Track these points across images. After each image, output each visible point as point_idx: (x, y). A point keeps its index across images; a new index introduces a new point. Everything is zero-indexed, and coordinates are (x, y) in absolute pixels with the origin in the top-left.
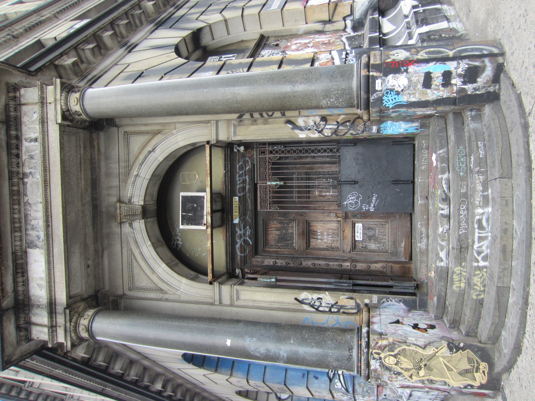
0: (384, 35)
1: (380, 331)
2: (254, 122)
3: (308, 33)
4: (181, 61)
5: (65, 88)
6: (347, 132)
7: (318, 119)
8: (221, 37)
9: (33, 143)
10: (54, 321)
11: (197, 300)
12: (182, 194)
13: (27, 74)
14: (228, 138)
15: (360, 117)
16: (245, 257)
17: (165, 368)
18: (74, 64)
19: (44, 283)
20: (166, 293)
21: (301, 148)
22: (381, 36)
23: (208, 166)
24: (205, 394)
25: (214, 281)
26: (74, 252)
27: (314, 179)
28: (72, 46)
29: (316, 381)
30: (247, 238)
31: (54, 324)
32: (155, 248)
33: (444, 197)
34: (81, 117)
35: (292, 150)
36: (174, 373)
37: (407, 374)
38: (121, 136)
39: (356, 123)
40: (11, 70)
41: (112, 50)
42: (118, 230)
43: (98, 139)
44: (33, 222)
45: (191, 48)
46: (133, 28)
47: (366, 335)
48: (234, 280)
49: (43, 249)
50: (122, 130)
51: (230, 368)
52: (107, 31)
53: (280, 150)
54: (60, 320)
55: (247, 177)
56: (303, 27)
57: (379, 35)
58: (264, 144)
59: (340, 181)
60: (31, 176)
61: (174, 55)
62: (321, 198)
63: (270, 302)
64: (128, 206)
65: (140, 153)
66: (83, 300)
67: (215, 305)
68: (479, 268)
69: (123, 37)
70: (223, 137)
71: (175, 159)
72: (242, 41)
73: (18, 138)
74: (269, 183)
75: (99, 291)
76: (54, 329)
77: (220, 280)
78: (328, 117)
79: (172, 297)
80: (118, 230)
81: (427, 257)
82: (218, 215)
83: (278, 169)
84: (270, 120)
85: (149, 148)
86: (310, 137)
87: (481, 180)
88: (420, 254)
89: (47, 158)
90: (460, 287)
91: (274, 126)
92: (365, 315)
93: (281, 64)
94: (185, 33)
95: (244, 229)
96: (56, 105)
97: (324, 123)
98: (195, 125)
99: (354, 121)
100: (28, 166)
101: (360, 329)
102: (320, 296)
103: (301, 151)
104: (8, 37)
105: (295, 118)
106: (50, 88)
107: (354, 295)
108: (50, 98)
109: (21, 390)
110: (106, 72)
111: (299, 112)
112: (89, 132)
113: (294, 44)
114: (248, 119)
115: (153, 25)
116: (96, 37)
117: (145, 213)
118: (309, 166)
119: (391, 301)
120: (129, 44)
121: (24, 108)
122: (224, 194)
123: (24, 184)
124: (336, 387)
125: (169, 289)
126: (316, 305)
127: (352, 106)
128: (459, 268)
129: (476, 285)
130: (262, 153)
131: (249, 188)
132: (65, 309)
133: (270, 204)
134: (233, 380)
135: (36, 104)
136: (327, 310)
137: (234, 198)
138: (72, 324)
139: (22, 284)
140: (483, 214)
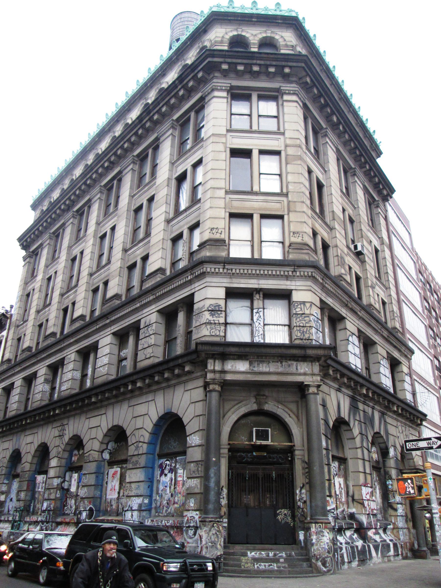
2: (303, 468)
3: (347, 486)
7: (305, 499)
8: (345, 435)
12: (270, 429)
19: (234, 369)
37: (209, 538)
42: (252, 395)
44: (261, 365)
46: (348, 387)
50: (299, 400)
55: (275, 460)
56: (351, 484)
72: (343, 447)
83: (280, 476)
91: (301, 478)
108: (315, 378)
113: (341, 480)
115: (352, 394)
121: (310, 363)
123: (277, 362)
135: (312, 371)
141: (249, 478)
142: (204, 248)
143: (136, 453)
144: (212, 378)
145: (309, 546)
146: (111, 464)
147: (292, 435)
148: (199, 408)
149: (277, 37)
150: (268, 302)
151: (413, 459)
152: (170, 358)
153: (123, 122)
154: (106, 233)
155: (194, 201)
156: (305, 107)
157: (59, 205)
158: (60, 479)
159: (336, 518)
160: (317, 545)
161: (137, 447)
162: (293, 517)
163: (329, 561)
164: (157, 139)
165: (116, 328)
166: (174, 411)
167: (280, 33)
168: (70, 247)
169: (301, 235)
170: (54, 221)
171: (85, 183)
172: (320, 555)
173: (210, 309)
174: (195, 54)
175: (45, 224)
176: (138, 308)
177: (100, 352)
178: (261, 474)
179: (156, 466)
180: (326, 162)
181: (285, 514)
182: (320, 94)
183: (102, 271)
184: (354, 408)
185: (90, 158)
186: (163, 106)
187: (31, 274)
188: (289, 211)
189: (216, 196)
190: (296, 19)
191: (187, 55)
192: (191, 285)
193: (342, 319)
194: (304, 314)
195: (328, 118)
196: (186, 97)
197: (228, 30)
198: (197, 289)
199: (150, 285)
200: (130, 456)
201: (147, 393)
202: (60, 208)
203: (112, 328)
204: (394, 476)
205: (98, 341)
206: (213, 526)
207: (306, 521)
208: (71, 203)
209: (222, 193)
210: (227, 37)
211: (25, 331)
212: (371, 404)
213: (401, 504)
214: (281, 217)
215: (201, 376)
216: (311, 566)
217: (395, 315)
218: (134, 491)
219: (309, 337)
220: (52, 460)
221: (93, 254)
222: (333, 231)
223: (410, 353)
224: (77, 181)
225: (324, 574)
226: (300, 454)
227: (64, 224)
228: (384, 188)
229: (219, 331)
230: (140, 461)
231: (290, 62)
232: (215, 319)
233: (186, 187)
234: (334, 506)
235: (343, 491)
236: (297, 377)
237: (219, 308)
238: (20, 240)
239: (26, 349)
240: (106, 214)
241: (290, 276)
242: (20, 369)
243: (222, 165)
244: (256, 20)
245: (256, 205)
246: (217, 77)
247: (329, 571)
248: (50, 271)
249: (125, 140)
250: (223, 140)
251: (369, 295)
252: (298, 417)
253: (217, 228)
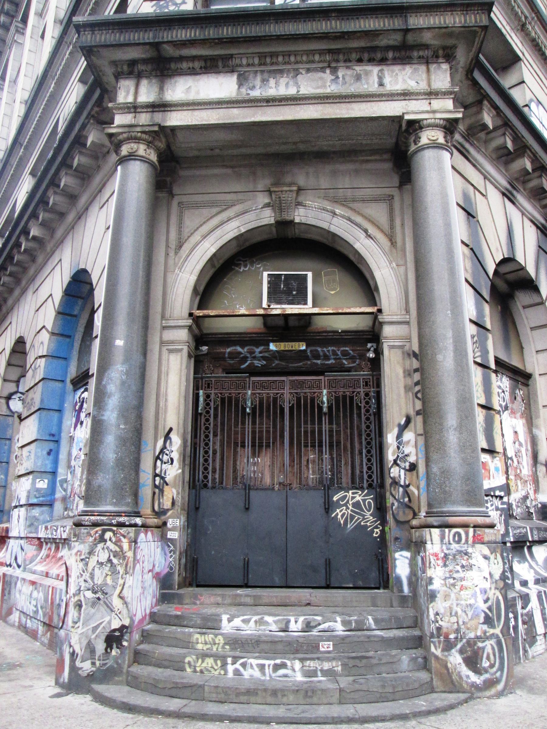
0: (530, 548)
1: (139, 541)
2: (408, 374)
4: (491, 268)
5: (450, 123)
6: (395, 498)
9: (376, 80)
10: (143, 110)
11: (168, 296)
12: (310, 275)
13: (469, 68)
14: (386, 338)
15: (415, 515)
16: (224, 359)
17: (61, 242)
18: (484, 127)
19: (192, 96)
20: (176, 253)
21: (373, 435)
22: (528, 544)
23: (348, 311)
24: (17, 292)
25: (193, 320)
26: (232, 134)
27: (331, 454)
28: (509, 120)
29: (45, 453)
30: (249, 362)
31: (139, 110)
32: (236, 238)
33: (313, 624)
34: (413, 144)
35: (370, 423)
36: (53, 252)
37: (86, 576)
38: (387, 191)
39: (407, 511)
40: (474, 50)
41: (506, 171)
43: (384, 161)
44: (272, 82)
45: (510, 277)
47: (133, 522)
48: (193, 345)
49: (238, 94)
50: (395, 192)
51: (61, 332)
52: (532, 163)
53: (370, 407)
54: (144, 118)
57: (530, 542)
59: (329, 489)
60: (333, 77)
61: (499, 258)
62: (305, 463)
63: (166, 395)
64: (294, 201)
66: (168, 146)
67: (162, 320)
68: (224, 665)
69: (524, 182)
70: (387, 331)
71: (356, 263)
72: (522, 348)
73: (383, 61)
74: (325, 392)
75: (177, 162)
76: (132, 110)
77: (194, 327)
78: (414, 472)
79: (171, 262)
80: (260, 187)
81: (230, 605)
82: (281, 322)
83: (344, 405)
84: (411, 394)
85: (372, 230)
86: (388, 449)
87: (336, 669)
88: (233, 595)
89: (358, 100)
90: (198, 643)
91: (403, 401)
92: (154, 521)
93: (487, 408)
94: (531, 270)
95: (262, 357)
96: (427, 112)
97: (407, 468)
98: (403, 293)
99: (410, 507)
100: (346, 74)
101: (137, 514)
102: (175, 462)
103: (368, 435)
104: (523, 19)
105: (413, 428)
106: (449, 104)
108: (437, 104)
109: (11, 16)
110: (474, 166)
111: (421, 435)
112: (393, 150)
113: (520, 424)
114: (411, 365)
116: (522, 149)
117: (284, 224)
118: (349, 446)
119: (171, 556)
120: (515, 192)
121: (423, 68)
122: (309, 329)
123: (323, 70)
124: (38, 480)
125: (181, 257)
126: (163, 456)
127: (430, 505)
128: (222, 642)
129: (203, 662)
130: (366, 383)
131: (317, 364)
132: (159, 125)
133: (296, 393)
134: (45, 336)
135: (429, 85)
136: (158, 471)
137: (304, 344)
138: (139, 134)
139: (191, 66)
140: (294, 670)
145: (422, 600)
159: (508, 514)
160: (447, 597)
162: (381, 510)
163: (488, 649)
172: (457, 631)
178: (287, 396)
179: (68, 406)
181: (357, 505)
206: (102, 539)
207: (415, 522)
216: (425, 666)
225: (473, 693)
234: (500, 480)
235: (523, 450)
247: (490, 684)
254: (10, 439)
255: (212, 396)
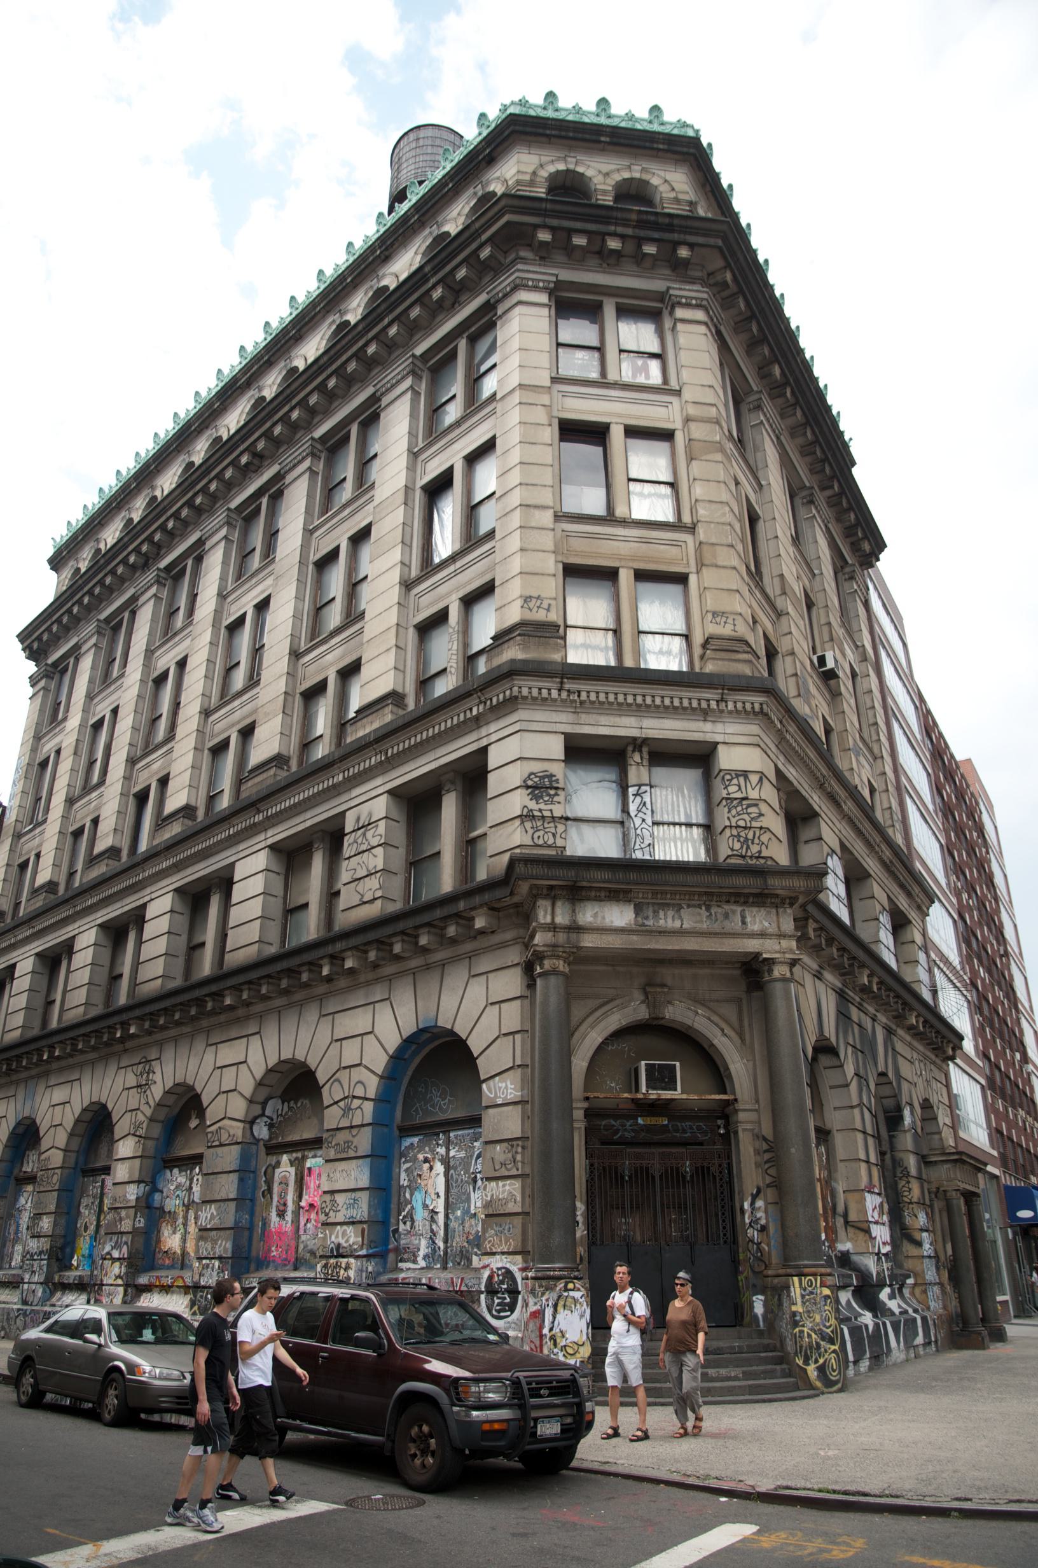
2: (757, 1152)
7: (763, 1222)
8: (828, 1078)
12: (678, 1064)
19: (599, 922)
34: (766, 974)
46: (837, 968)
54: (561, 937)
58: (729, 1157)
65: (720, 1016)
73: (745, 903)
83: (702, 1172)
94: (833, 1040)
107: (586, 1262)
108: (785, 943)
115: (840, 985)
123: (699, 906)
141: (630, 1177)
142: (512, 642)
143: (345, 1123)
144: (549, 942)
146: (275, 1148)
147: (730, 1076)
148: (513, 1016)
149: (655, 181)
150: (661, 774)
151: (940, 1133)
152: (417, 904)
153: (282, 364)
154: (245, 614)
155: (473, 538)
156: (719, 337)
157: (125, 553)
158: (142, 1185)
161: (347, 1111)
164: (374, 399)
165: (277, 834)
166: (444, 1022)
167: (662, 173)
168: (149, 653)
169: (730, 621)
170: (110, 592)
171: (190, 504)
173: (530, 783)
174: (467, 210)
175: (86, 600)
176: (339, 784)
177: (149, 930)
178: (657, 1169)
180: (760, 465)
182: (749, 314)
183: (236, 703)
184: (843, 1015)
185: (198, 448)
186: (390, 324)
187: (50, 717)
188: (701, 565)
189: (533, 524)
190: (696, 141)
191: (447, 211)
192: (479, 727)
193: (811, 816)
194: (746, 798)
195: (763, 373)
196: (448, 303)
197: (544, 159)
198: (494, 738)
199: (367, 731)
200: (328, 1130)
201: (368, 983)
202: (124, 561)
203: (270, 833)
204: (913, 1171)
205: (232, 866)
208: (155, 550)
209: (547, 518)
210: (544, 174)
211: (40, 845)
212: (871, 1010)
213: (926, 1231)
214: (681, 579)
215: (515, 941)
217: (895, 817)
218: (343, 1211)
219: (760, 852)
220: (121, 1142)
221: (212, 665)
222: (784, 619)
223: (927, 902)
224: (165, 503)
226: (749, 1120)
227: (134, 599)
228: (865, 537)
229: (554, 835)
230: (355, 1140)
231: (691, 234)
232: (542, 806)
233: (448, 513)
236: (732, 941)
237: (551, 782)
238: (23, 636)
239: (42, 887)
240: (241, 573)
241: (713, 711)
242: (30, 932)
243: (547, 455)
244: (608, 139)
245: (624, 548)
246: (524, 260)
248: (99, 708)
249: (294, 402)
250: (545, 399)
251: (852, 769)
252: (741, 1035)
253: (538, 598)
254: (71, 1191)
255: (596, 1165)
